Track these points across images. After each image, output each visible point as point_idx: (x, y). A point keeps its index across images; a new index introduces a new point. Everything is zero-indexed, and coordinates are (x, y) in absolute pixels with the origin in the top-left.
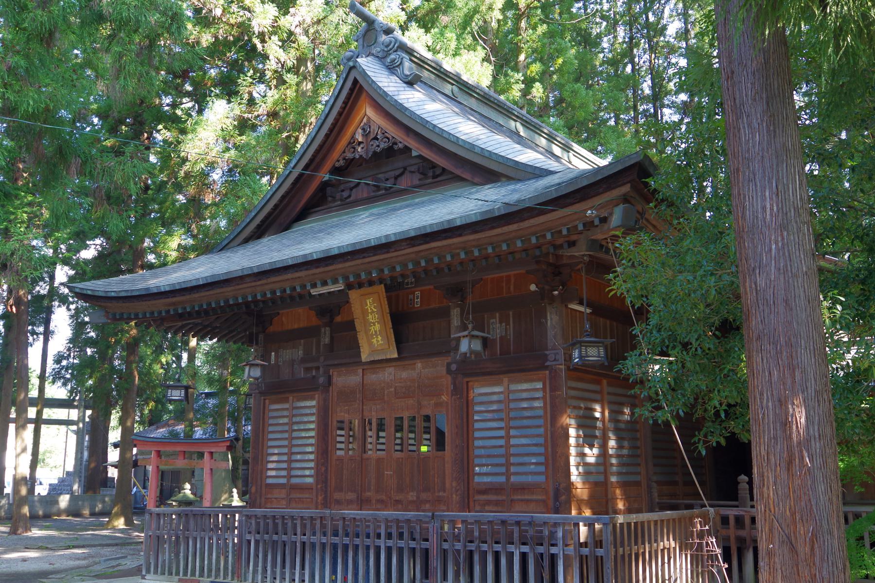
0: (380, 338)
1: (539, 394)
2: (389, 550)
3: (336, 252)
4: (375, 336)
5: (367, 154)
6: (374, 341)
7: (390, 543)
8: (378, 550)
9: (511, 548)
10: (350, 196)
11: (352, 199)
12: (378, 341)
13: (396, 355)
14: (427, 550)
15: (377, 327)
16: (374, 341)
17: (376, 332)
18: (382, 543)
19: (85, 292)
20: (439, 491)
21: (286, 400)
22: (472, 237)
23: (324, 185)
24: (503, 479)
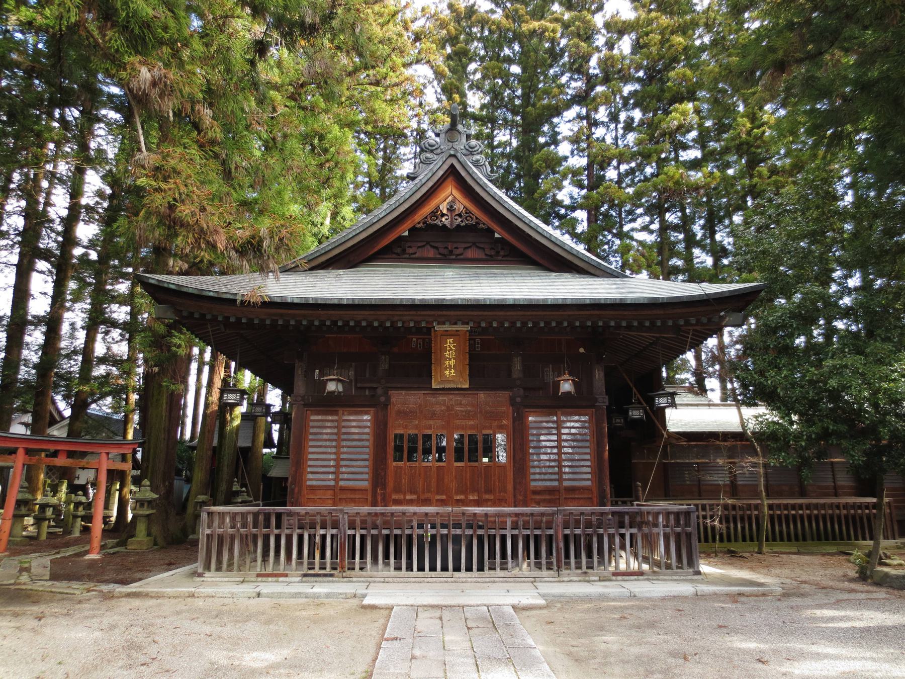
0: (453, 371)
1: (369, 424)
2: (514, 539)
3: (512, 302)
4: (450, 367)
5: (451, 225)
6: (447, 372)
7: (516, 532)
8: (503, 538)
9: (623, 531)
10: (415, 253)
11: (416, 256)
12: (449, 373)
13: (467, 386)
14: (551, 536)
15: (452, 362)
16: (447, 372)
17: (450, 366)
18: (508, 533)
19: (161, 285)
20: (500, 492)
21: (335, 413)
22: (612, 312)
23: (401, 239)
24: (556, 483)
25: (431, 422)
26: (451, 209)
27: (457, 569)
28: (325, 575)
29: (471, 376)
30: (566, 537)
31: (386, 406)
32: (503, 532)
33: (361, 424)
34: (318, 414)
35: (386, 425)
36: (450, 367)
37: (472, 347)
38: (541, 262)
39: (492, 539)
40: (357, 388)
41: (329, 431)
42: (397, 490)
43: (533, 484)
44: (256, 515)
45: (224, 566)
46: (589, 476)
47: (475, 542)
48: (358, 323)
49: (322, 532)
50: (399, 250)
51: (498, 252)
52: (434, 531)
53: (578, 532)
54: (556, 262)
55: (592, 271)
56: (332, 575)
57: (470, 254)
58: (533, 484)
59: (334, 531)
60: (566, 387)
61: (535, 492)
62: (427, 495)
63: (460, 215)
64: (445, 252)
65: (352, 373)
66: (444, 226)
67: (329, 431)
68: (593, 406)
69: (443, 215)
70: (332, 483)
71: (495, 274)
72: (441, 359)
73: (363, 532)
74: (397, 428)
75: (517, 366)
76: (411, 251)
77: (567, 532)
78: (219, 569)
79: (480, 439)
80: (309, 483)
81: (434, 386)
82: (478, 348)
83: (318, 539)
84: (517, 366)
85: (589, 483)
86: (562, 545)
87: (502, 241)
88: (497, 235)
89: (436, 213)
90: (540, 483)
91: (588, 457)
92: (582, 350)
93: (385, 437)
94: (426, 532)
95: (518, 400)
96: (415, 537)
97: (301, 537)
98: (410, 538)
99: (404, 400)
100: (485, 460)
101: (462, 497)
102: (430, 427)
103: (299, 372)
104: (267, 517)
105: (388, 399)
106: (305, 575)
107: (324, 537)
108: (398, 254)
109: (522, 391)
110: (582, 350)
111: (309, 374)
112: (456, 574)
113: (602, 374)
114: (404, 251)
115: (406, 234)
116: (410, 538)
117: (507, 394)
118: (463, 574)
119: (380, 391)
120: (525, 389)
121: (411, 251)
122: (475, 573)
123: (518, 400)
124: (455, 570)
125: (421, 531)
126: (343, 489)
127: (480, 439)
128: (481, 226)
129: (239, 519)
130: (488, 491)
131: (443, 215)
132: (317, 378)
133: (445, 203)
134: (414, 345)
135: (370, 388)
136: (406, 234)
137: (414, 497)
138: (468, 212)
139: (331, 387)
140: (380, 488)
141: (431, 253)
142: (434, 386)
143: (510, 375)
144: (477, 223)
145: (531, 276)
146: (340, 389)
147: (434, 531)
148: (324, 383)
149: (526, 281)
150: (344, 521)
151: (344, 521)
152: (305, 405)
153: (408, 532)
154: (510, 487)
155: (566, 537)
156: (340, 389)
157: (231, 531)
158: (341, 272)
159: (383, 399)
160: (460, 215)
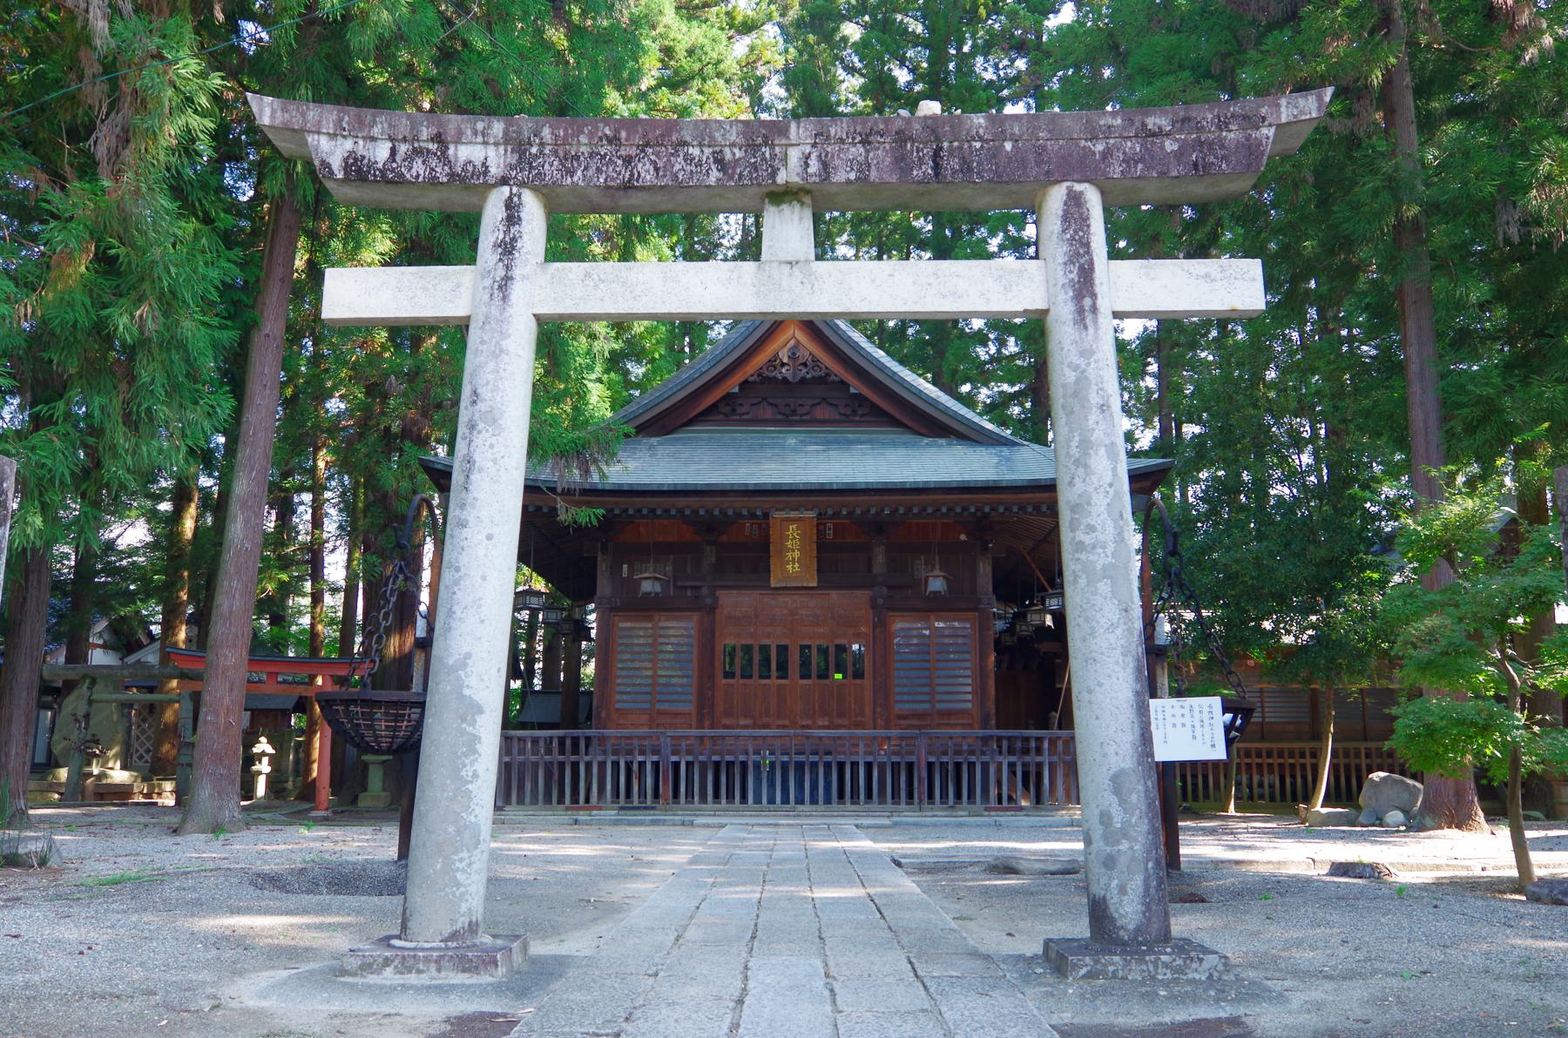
4: (793, 557)
8: (855, 765)
15: (797, 554)
21: (650, 618)
23: (729, 396)
24: (927, 706)
25: (770, 630)
26: (793, 357)
27: (800, 801)
28: (646, 808)
29: (819, 571)
30: (930, 765)
31: (712, 609)
32: (854, 759)
33: (678, 631)
34: (627, 621)
35: (713, 632)
36: (793, 557)
37: (821, 533)
38: (910, 424)
39: (841, 765)
40: (676, 588)
41: (641, 641)
42: (728, 714)
43: (898, 707)
44: (562, 741)
45: (528, 799)
46: (970, 697)
47: (821, 770)
48: (680, 511)
49: (641, 758)
50: (727, 409)
51: (854, 412)
52: (773, 758)
53: (945, 759)
54: (931, 426)
55: (973, 436)
56: (653, 808)
57: (820, 413)
58: (898, 707)
59: (655, 758)
60: (937, 584)
61: (900, 717)
62: (765, 720)
63: (805, 365)
64: (787, 411)
65: (669, 568)
66: (785, 379)
67: (641, 641)
68: (975, 609)
69: (783, 365)
70: (647, 706)
71: (851, 442)
72: (783, 550)
73: (690, 758)
74: (729, 639)
75: (880, 558)
76: (744, 410)
77: (932, 759)
78: (521, 801)
79: (724, 800)
80: (618, 706)
81: (773, 585)
82: (830, 533)
83: (635, 767)
84: (880, 558)
85: (969, 705)
86: (924, 774)
87: (859, 397)
88: (852, 390)
89: (774, 362)
90: (906, 706)
91: (969, 673)
92: (963, 537)
93: (713, 649)
94: (764, 758)
95: (880, 601)
96: (750, 764)
97: (616, 764)
98: (744, 765)
99: (735, 602)
100: (838, 676)
101: (809, 722)
102: (768, 636)
103: (602, 568)
104: (575, 740)
105: (716, 599)
106: (622, 808)
107: (642, 764)
108: (726, 415)
109: (885, 589)
110: (963, 537)
111: (615, 570)
112: (800, 807)
113: (989, 569)
114: (734, 410)
115: (736, 390)
116: (744, 765)
117: (866, 594)
118: (807, 807)
119: (704, 591)
120: (889, 587)
121: (744, 410)
122: (821, 807)
123: (880, 601)
124: (797, 802)
125: (757, 758)
126: (660, 713)
127: (724, 800)
128: (833, 378)
129: (542, 743)
130: (841, 715)
131: (783, 365)
132: (625, 575)
133: (785, 350)
134: (747, 532)
135: (692, 588)
136: (736, 390)
137: (749, 722)
138: (815, 360)
139: (647, 587)
140: (706, 711)
141: (769, 413)
142: (773, 585)
143: (870, 570)
144: (828, 375)
145: (894, 444)
146: (658, 589)
147: (773, 758)
148: (638, 583)
149: (887, 452)
150: (666, 743)
151: (666, 743)
152: (612, 609)
153: (742, 758)
154: (868, 710)
155: (930, 765)
156: (658, 589)
157: (533, 758)
158: (654, 440)
159: (709, 601)
160: (805, 365)
